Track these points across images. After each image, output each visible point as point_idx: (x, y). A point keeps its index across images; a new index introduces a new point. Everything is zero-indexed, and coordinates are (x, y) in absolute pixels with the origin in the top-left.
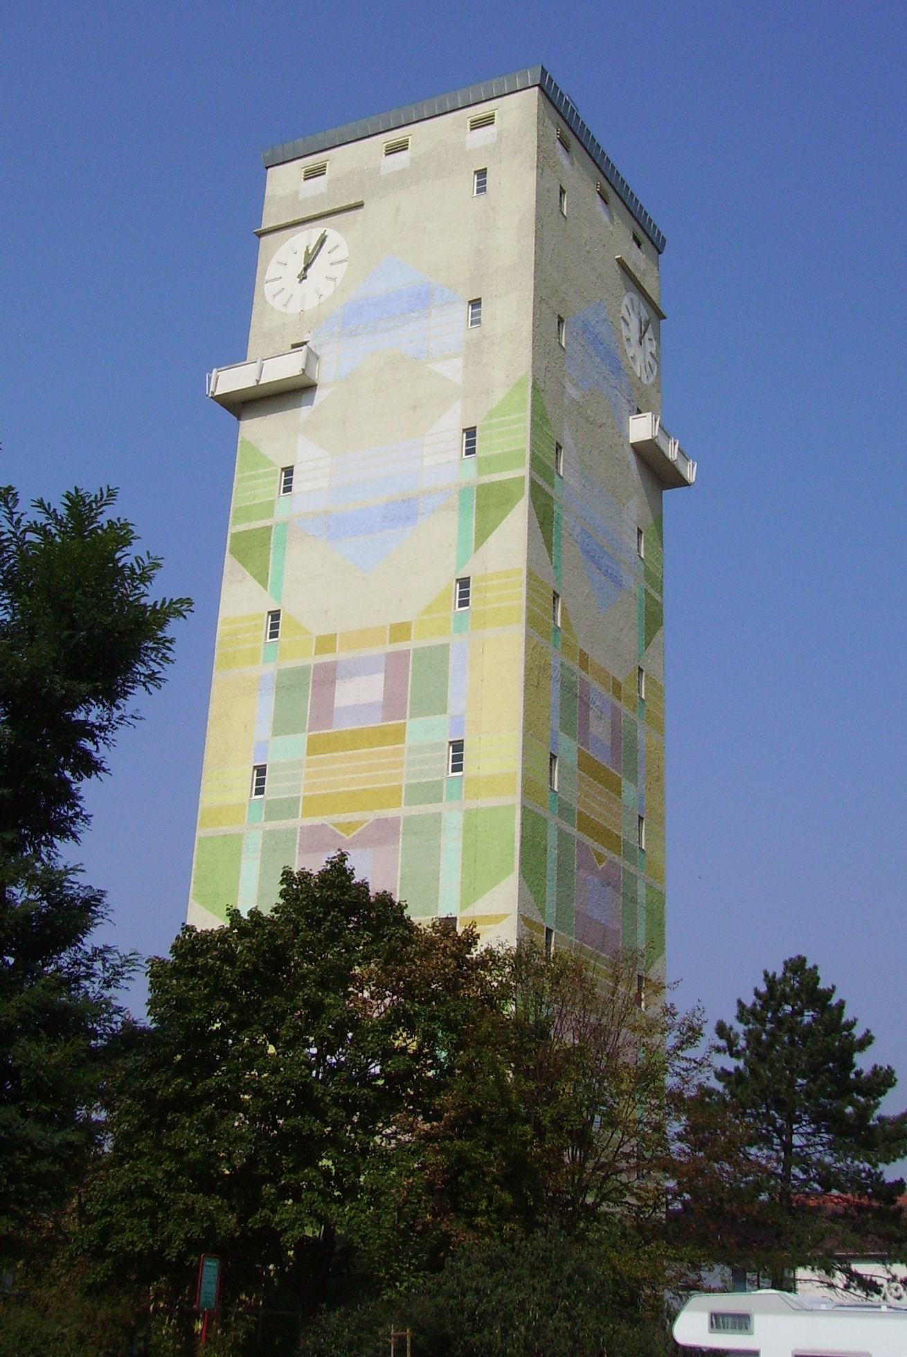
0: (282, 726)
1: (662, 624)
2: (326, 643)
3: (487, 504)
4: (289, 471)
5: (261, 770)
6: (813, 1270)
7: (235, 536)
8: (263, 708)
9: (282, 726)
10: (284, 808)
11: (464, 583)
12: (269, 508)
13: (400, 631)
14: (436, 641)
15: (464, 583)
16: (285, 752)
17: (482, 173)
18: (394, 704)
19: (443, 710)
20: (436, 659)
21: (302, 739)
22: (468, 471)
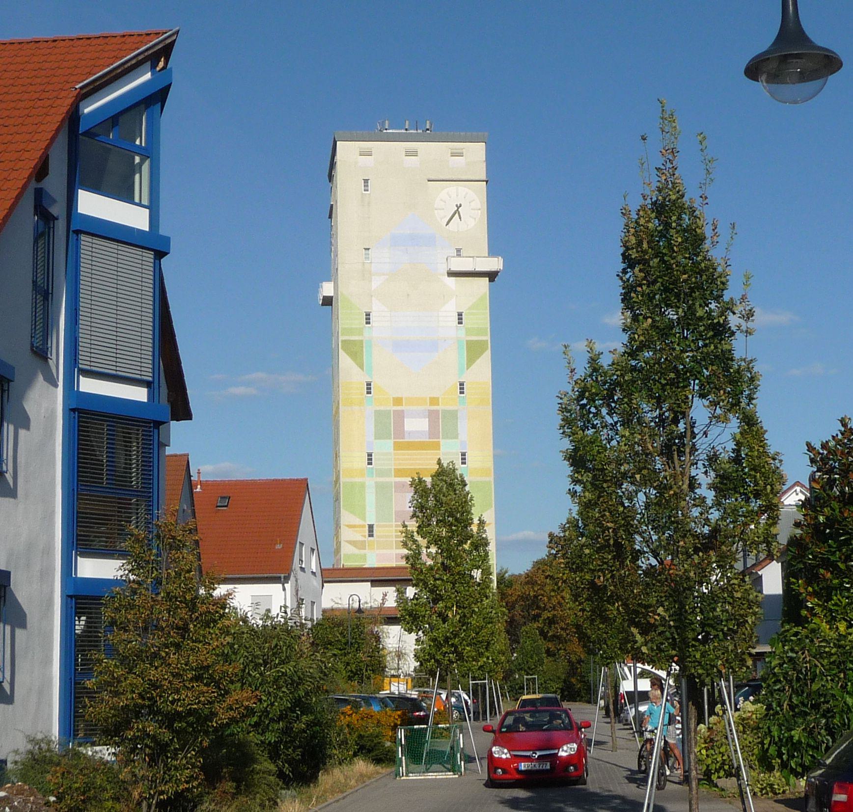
0: (378, 436)
1: (25, 615)
2: (398, 401)
3: (473, 351)
4: (368, 314)
5: (370, 455)
6: (797, 525)
7: (342, 341)
8: (370, 427)
9: (378, 436)
10: (381, 473)
11: (462, 384)
12: (360, 332)
13: (434, 401)
14: (455, 408)
15: (462, 384)
16: (384, 448)
17: (366, 181)
18: (433, 431)
19: (456, 437)
20: (452, 416)
21: (391, 442)
22: (462, 332)
